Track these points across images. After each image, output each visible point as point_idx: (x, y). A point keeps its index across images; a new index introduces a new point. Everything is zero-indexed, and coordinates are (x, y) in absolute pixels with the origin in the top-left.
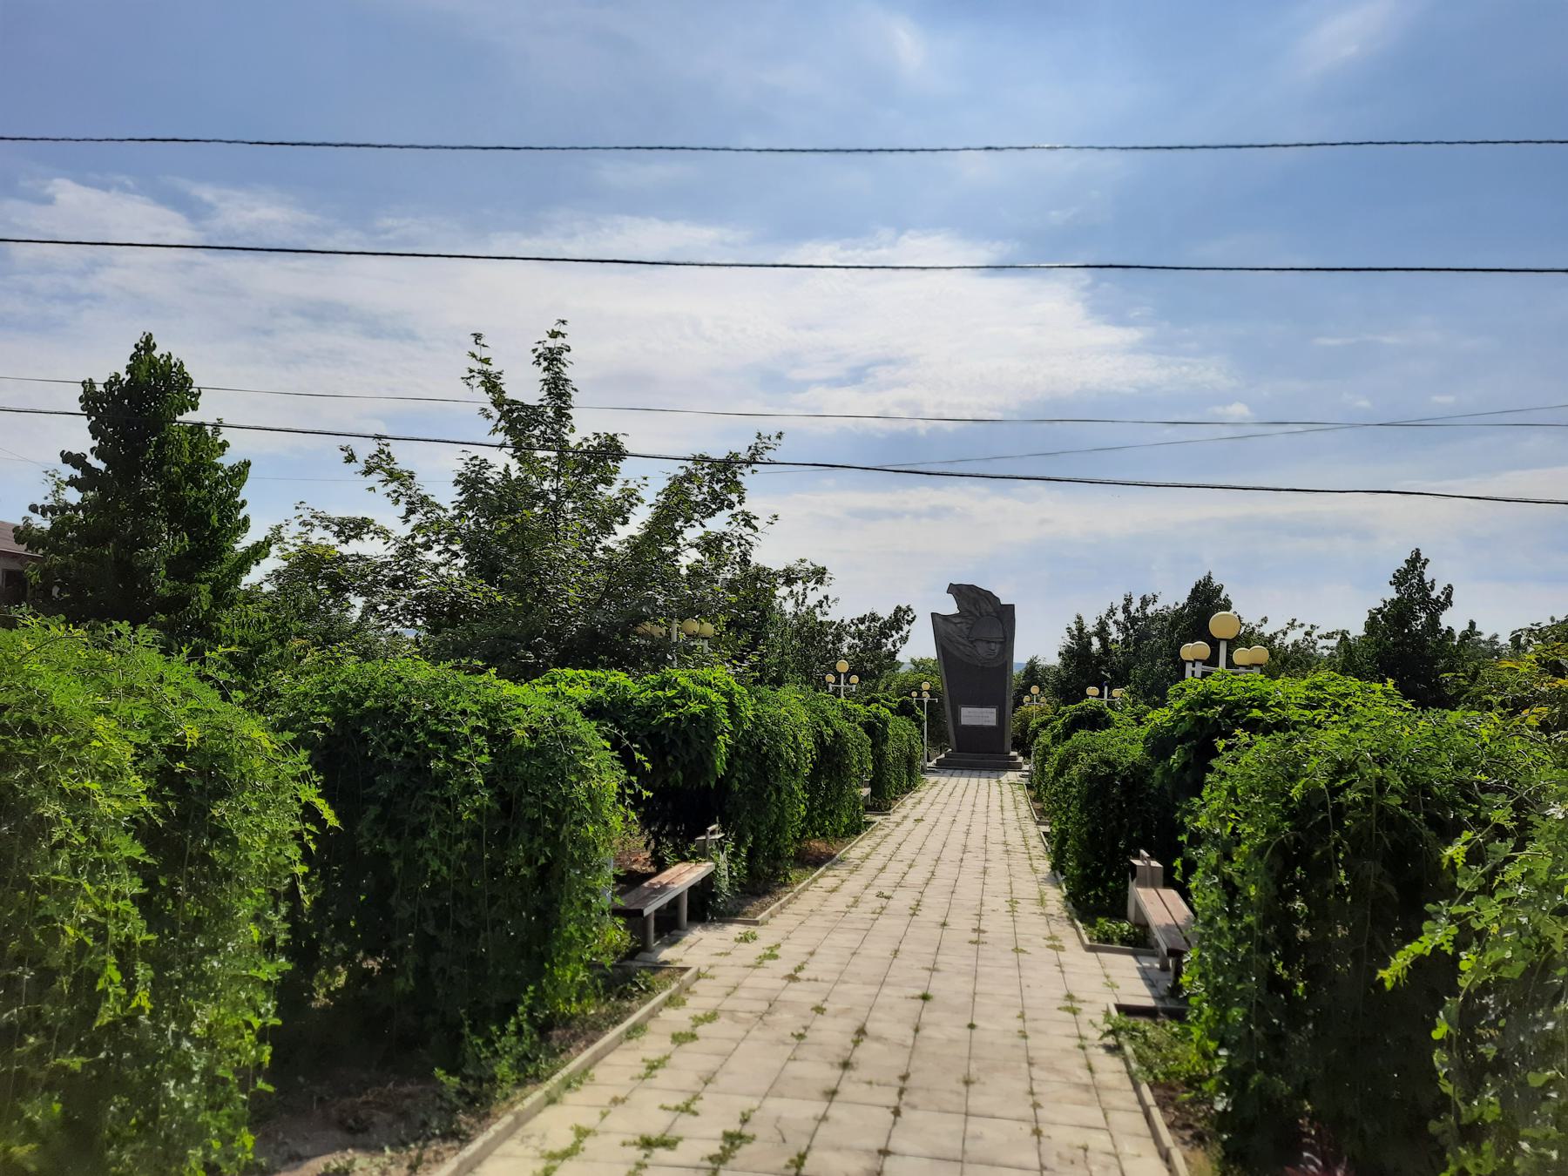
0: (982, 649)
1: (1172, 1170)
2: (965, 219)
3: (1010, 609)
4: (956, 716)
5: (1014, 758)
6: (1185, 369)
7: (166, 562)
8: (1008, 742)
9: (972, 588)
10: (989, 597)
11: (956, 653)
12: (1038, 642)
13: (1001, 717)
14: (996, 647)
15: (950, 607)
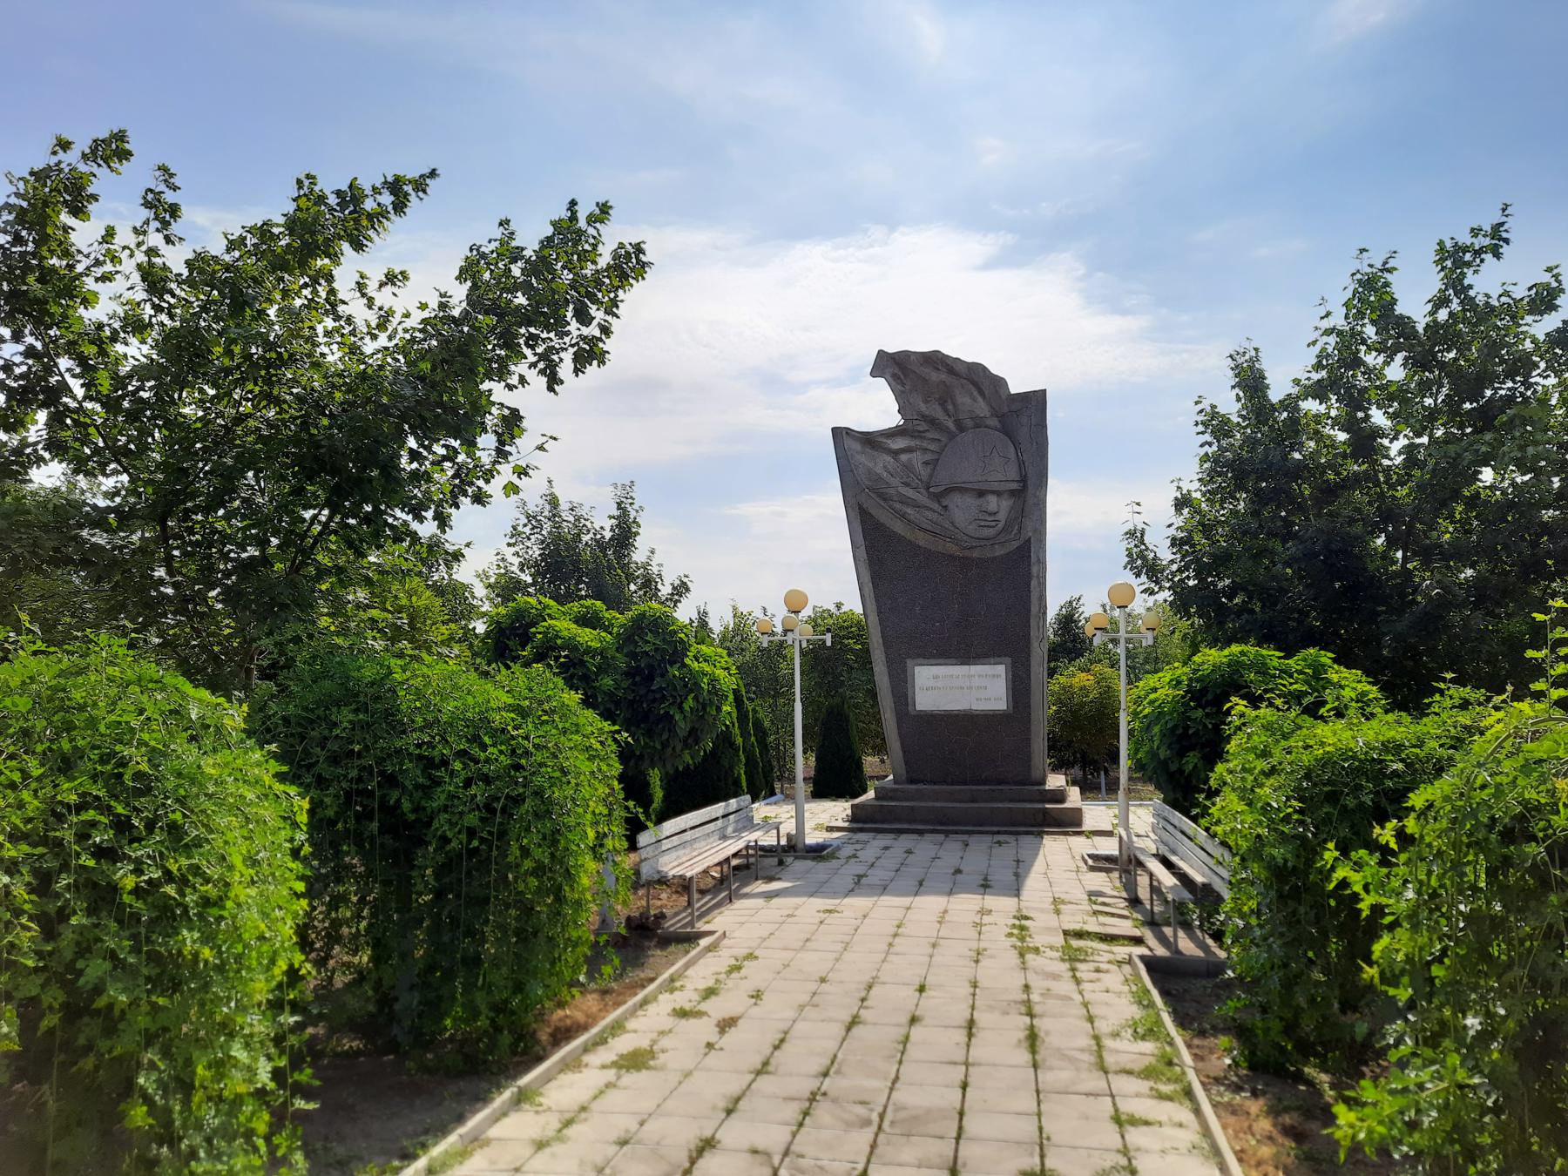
0: (962, 510)
1: (1223, 1167)
2: (969, 213)
3: (1035, 402)
4: (902, 694)
5: (1059, 796)
6: (1185, 356)
7: (44, 449)
8: (1039, 745)
9: (935, 360)
10: (977, 378)
11: (899, 527)
12: (1108, 522)
13: (1019, 688)
14: (1000, 506)
15: (878, 409)
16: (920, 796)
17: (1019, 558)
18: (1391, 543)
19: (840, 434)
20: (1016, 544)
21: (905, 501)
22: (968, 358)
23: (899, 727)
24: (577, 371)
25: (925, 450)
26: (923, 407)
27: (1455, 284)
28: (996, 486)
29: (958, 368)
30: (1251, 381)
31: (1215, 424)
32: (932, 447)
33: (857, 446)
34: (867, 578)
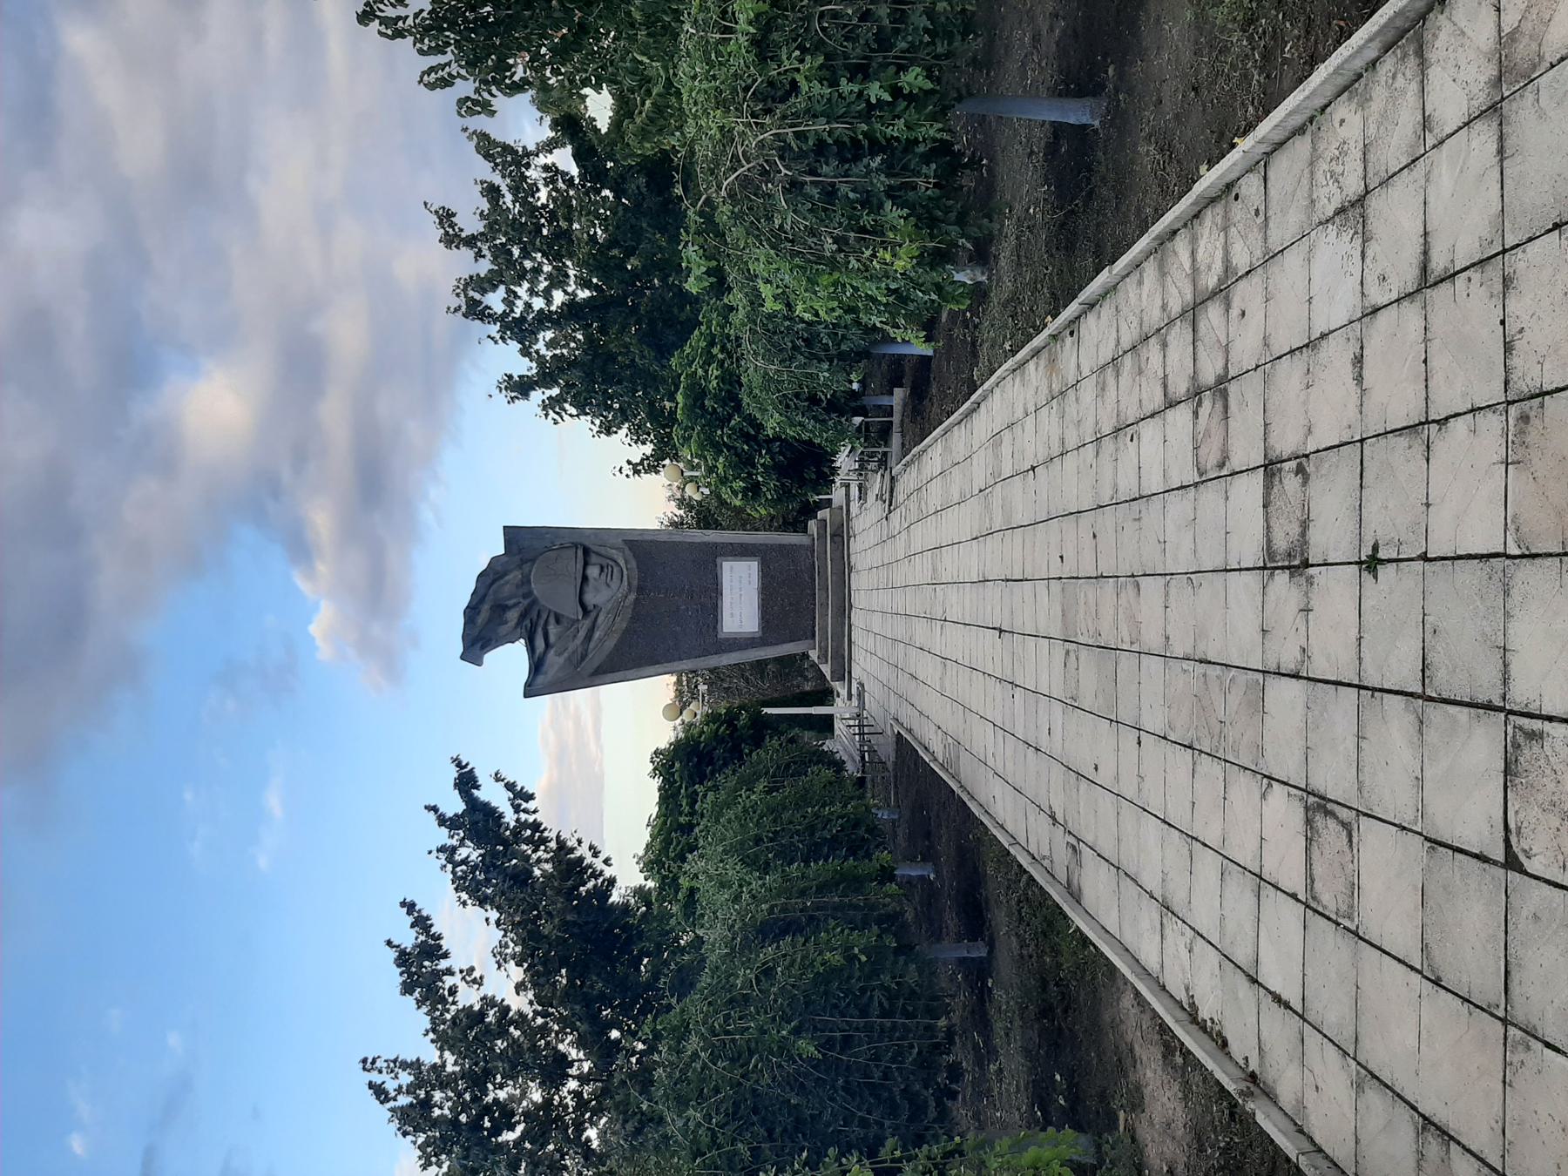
3: (513, 535)
9: (471, 612)
10: (490, 578)
15: (511, 659)
16: (824, 630)
17: (638, 545)
18: (514, 1042)
19: (530, 690)
20: (627, 551)
21: (589, 637)
22: (471, 586)
23: (772, 644)
24: (371, 1085)
25: (546, 622)
26: (512, 624)
27: (470, 242)
28: (580, 566)
29: (482, 592)
30: (520, 388)
31: (550, 405)
32: (544, 616)
33: (540, 679)
34: (652, 669)
